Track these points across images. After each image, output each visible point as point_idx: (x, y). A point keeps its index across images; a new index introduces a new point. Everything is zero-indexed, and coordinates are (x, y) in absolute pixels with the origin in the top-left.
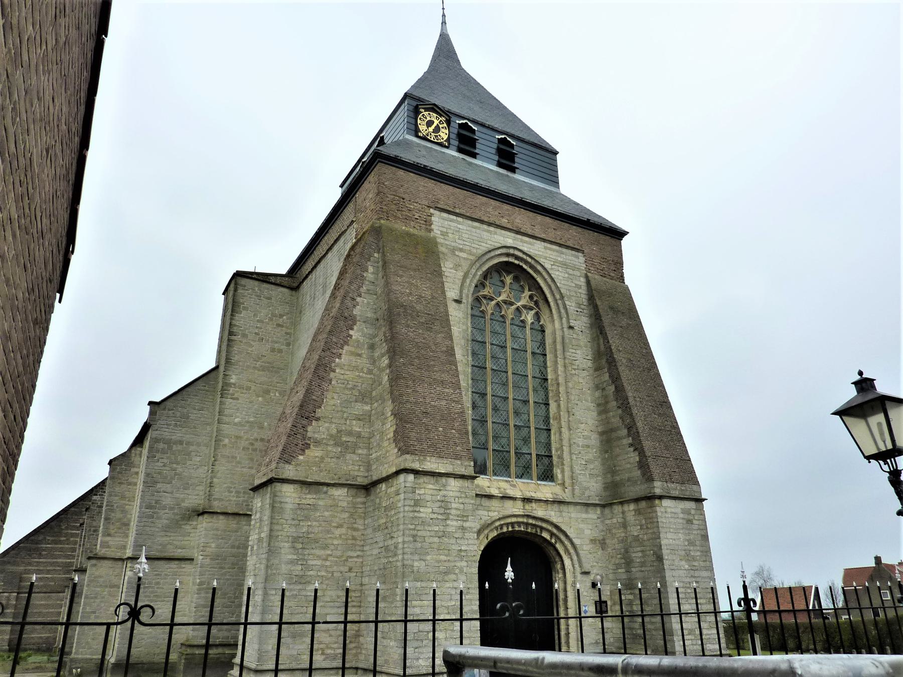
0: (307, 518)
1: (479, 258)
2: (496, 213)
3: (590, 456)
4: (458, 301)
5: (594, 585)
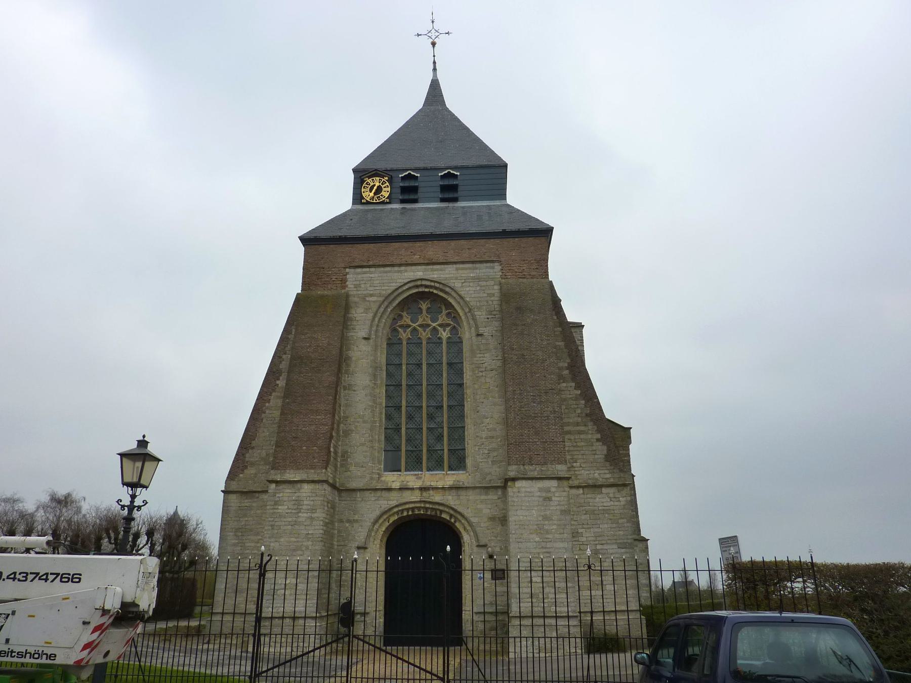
0: (245, 515)
1: (387, 298)
2: (409, 253)
3: (494, 445)
5: (491, 557)
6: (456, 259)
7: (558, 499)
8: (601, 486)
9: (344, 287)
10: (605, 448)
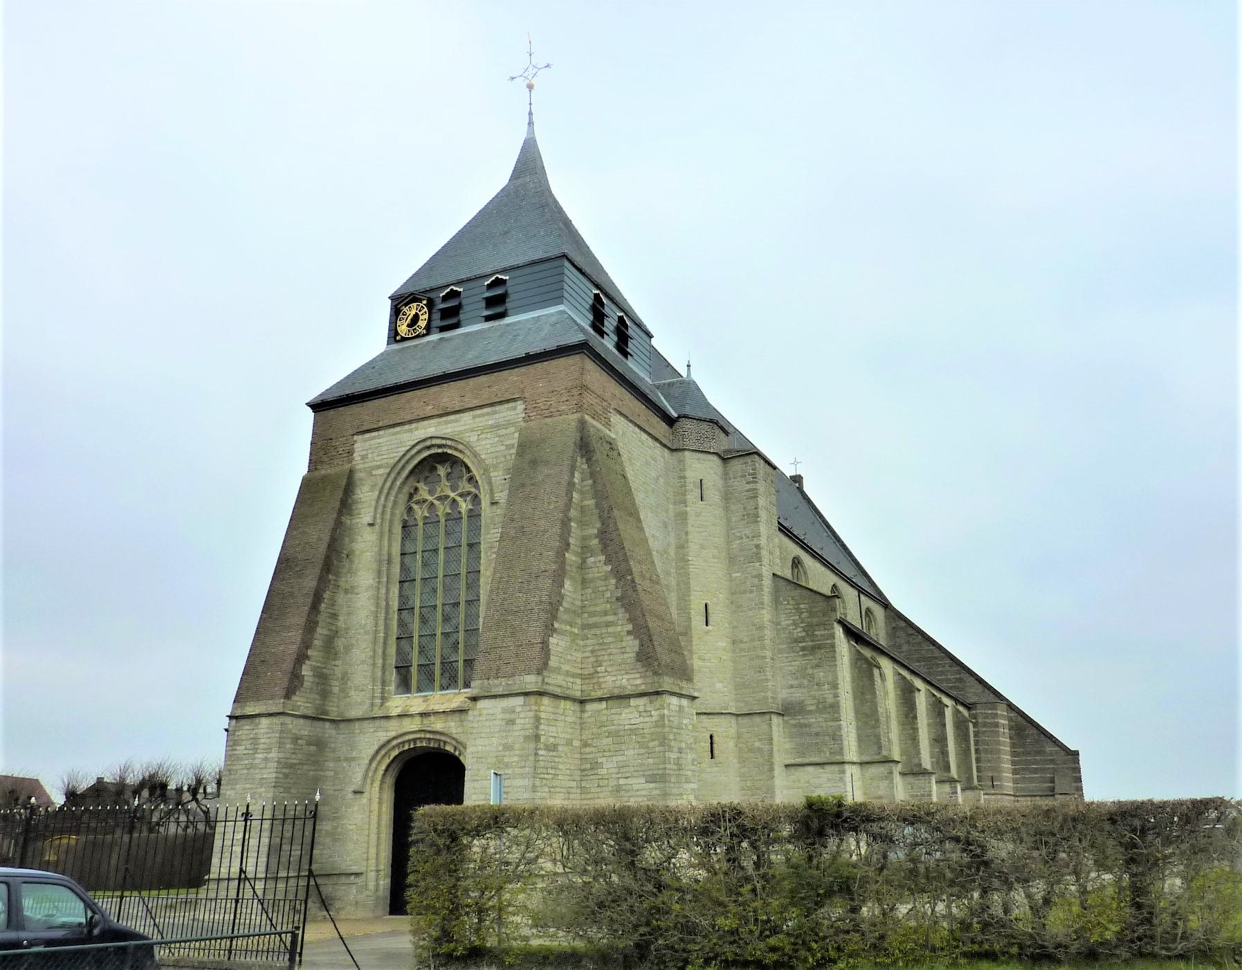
4: (371, 525)
6: (476, 403)
7: (522, 721)
8: (629, 697)
9: (350, 461)
10: (637, 642)
